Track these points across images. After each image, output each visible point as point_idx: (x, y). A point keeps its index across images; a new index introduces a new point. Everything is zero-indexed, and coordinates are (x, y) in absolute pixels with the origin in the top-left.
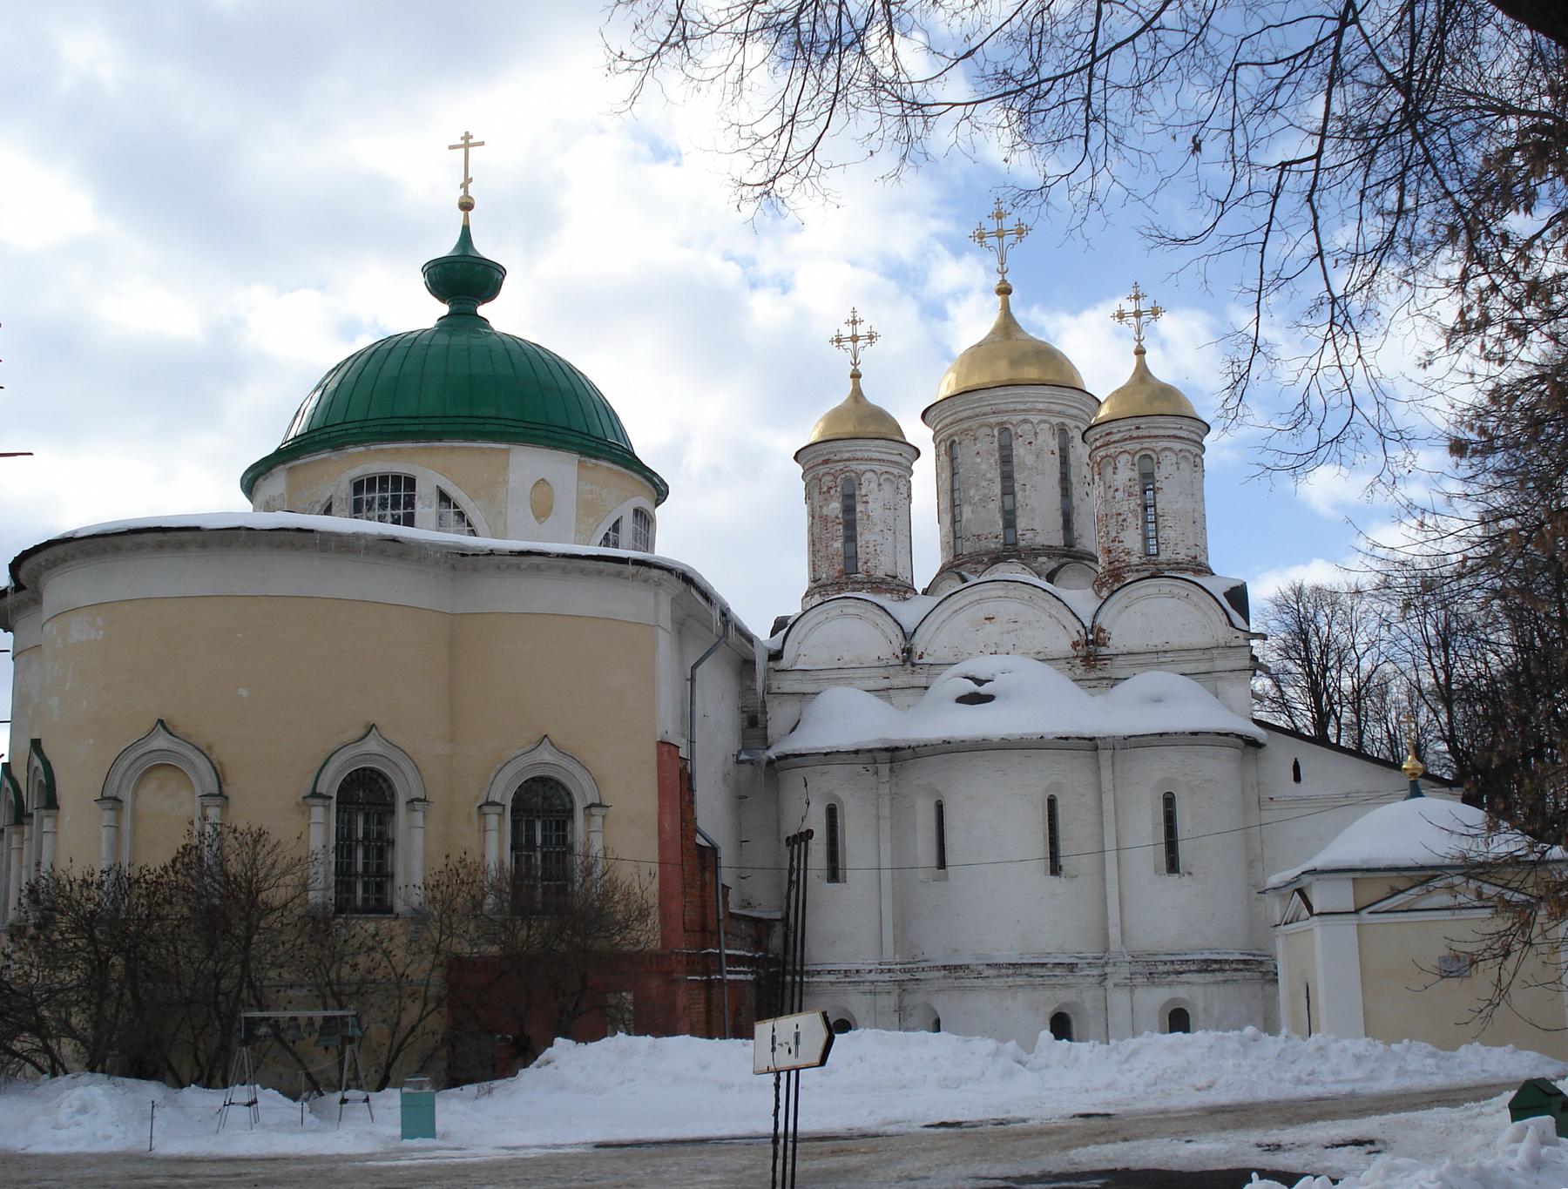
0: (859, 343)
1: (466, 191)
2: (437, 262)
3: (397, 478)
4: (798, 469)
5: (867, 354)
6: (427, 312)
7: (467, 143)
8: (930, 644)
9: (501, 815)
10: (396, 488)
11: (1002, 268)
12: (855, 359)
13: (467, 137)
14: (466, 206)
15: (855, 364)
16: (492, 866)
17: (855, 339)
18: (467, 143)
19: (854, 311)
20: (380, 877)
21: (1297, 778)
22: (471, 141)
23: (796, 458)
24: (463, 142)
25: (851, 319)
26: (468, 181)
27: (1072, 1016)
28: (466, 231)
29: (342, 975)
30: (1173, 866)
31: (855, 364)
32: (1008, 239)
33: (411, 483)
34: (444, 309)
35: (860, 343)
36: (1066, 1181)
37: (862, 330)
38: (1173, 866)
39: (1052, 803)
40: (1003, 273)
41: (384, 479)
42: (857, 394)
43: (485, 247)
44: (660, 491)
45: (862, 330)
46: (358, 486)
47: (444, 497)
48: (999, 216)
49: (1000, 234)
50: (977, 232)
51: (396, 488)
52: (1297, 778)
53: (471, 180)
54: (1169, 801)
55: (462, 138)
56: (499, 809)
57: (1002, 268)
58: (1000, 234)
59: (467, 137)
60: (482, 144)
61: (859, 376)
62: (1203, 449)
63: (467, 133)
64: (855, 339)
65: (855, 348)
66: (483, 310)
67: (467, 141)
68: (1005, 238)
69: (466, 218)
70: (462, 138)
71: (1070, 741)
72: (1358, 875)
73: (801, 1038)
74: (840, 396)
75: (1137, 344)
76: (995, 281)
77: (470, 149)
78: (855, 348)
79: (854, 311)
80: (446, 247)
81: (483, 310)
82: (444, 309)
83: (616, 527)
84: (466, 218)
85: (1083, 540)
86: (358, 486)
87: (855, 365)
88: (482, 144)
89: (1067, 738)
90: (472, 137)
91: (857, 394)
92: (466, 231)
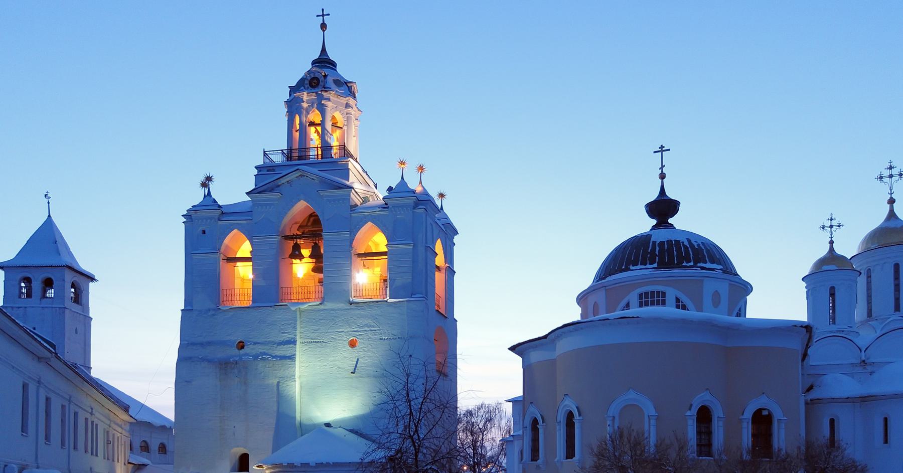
0: (833, 228)
1: (662, 171)
3: (658, 292)
4: (804, 284)
6: (645, 224)
7: (662, 149)
9: (748, 423)
11: (891, 192)
12: (891, 190)
13: (662, 147)
14: (662, 176)
16: (652, 444)
17: (831, 227)
18: (662, 149)
20: (709, 445)
22: (663, 149)
23: (803, 279)
24: (660, 150)
26: (663, 166)
33: (664, 294)
34: (654, 222)
35: (833, 229)
37: (835, 223)
41: (653, 292)
42: (832, 249)
43: (671, 194)
45: (835, 223)
46: (640, 296)
47: (678, 300)
50: (879, 176)
51: (652, 297)
55: (660, 148)
57: (891, 192)
59: (662, 147)
60: (669, 150)
61: (833, 242)
63: (662, 145)
64: (831, 227)
66: (670, 221)
67: (662, 150)
69: (662, 182)
70: (660, 148)
71: (849, 399)
74: (824, 251)
77: (663, 153)
80: (653, 196)
81: (670, 221)
82: (654, 222)
83: (740, 309)
84: (662, 182)
86: (640, 296)
87: (831, 238)
88: (669, 150)
89: (834, 399)
90: (664, 147)
91: (832, 249)
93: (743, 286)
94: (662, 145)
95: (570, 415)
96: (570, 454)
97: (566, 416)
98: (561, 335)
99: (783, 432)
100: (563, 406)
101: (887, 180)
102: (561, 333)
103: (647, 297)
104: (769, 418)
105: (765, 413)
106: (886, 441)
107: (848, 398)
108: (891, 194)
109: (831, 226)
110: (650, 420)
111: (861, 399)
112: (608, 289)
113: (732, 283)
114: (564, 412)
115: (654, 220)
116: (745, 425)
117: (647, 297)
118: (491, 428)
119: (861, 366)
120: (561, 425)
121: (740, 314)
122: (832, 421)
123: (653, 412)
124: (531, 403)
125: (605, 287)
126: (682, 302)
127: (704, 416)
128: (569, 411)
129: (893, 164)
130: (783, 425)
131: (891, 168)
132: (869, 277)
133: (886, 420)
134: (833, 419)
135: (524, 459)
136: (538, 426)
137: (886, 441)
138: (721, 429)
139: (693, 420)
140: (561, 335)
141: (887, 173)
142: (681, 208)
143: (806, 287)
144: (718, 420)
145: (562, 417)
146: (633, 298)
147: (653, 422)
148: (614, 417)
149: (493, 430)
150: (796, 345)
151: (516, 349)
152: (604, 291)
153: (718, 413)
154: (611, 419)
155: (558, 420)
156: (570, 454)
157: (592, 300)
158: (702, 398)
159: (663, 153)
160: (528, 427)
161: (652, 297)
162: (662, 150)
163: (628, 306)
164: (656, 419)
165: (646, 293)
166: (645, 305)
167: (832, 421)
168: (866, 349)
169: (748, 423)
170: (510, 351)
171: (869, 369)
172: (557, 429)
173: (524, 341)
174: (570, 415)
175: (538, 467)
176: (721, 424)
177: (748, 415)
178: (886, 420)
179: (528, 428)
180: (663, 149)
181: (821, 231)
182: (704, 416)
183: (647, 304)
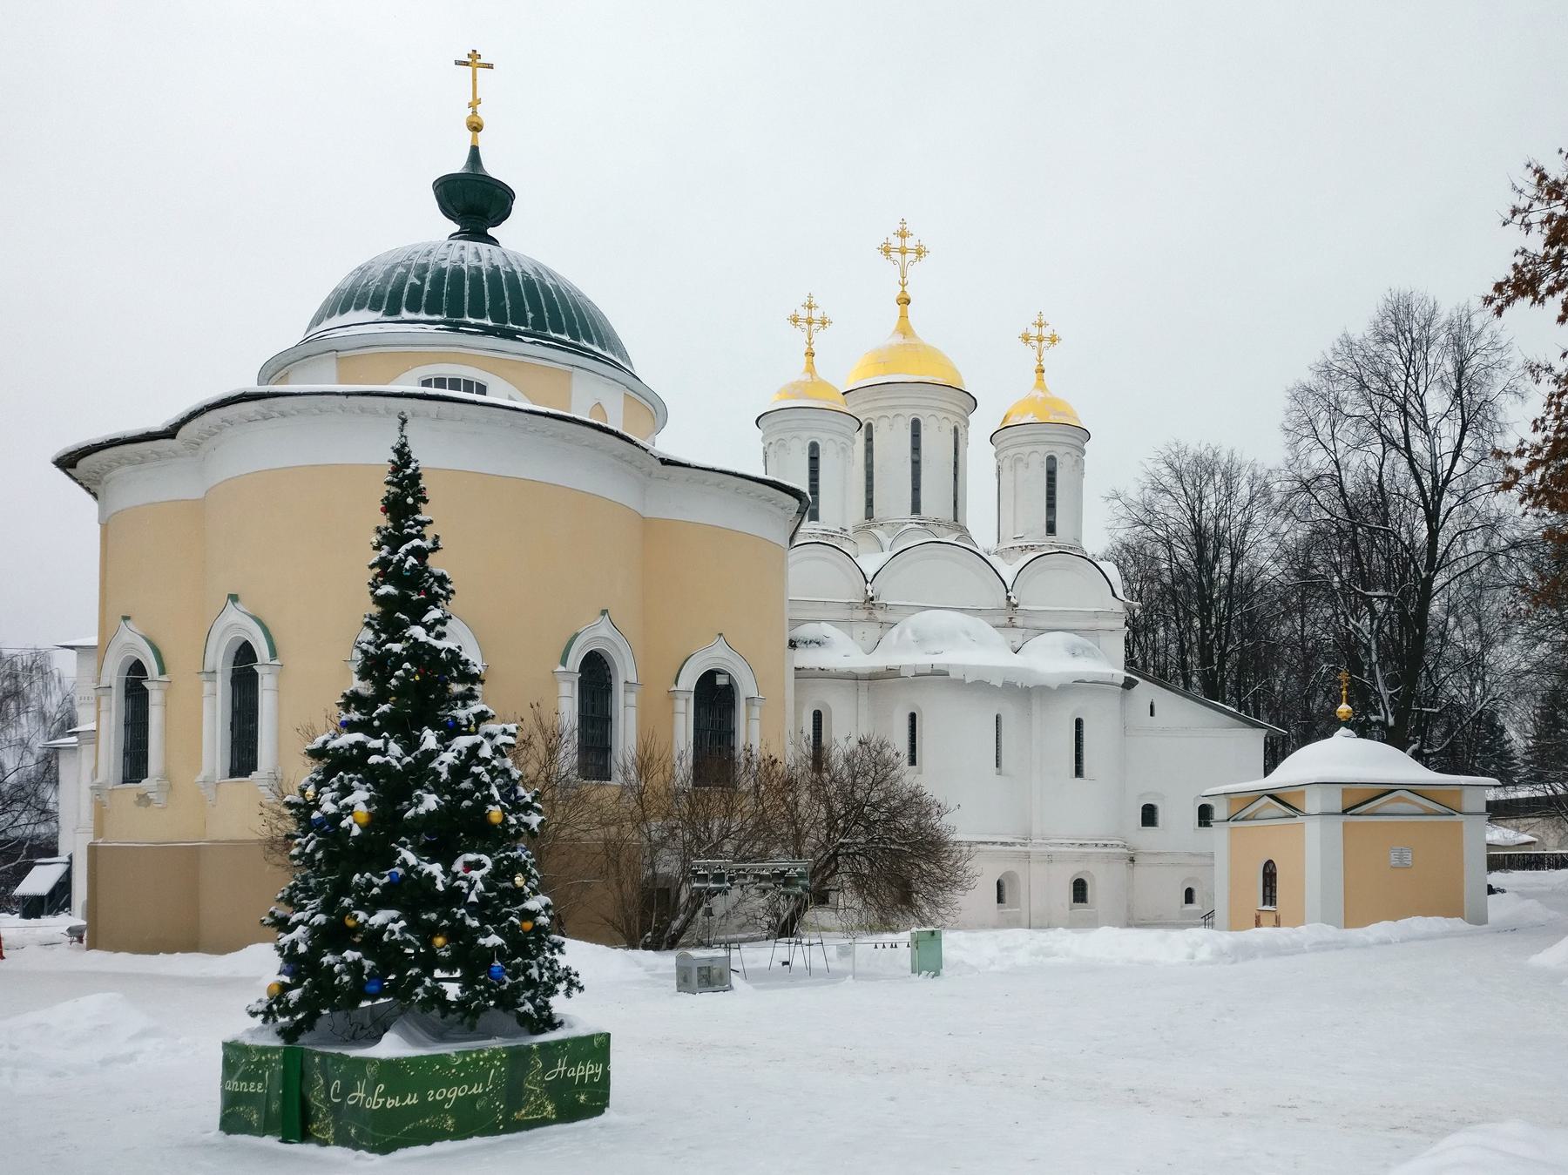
1: (475, 113)
2: (441, 181)
7: (473, 61)
8: (888, 592)
12: (810, 339)
13: (474, 55)
15: (810, 344)
18: (473, 61)
19: (810, 296)
21: (1152, 714)
24: (470, 60)
28: (475, 151)
29: (1414, 336)
30: (1079, 772)
31: (810, 344)
38: (1079, 772)
40: (903, 286)
43: (493, 167)
45: (910, 243)
48: (903, 235)
49: (903, 252)
54: (1079, 723)
56: (687, 696)
58: (903, 252)
59: (474, 55)
60: (490, 66)
62: (1084, 452)
65: (810, 329)
66: (491, 231)
68: (907, 255)
69: (475, 138)
72: (1344, 786)
73: (1156, 708)
78: (810, 329)
79: (810, 296)
80: (457, 164)
81: (491, 231)
85: (1357, 337)
88: (490, 66)
91: (904, 329)
92: (475, 151)
93: (651, 408)
95: (245, 653)
96: (243, 759)
98: (220, 428)
99: (755, 725)
101: (896, 256)
104: (730, 691)
105: (721, 681)
108: (903, 286)
109: (809, 320)
112: (342, 358)
113: (631, 393)
114: (227, 641)
118: (18, 714)
119: (864, 608)
124: (126, 618)
125: (337, 351)
130: (756, 712)
133: (913, 717)
134: (819, 711)
136: (146, 684)
138: (632, 712)
139: (573, 683)
140: (220, 428)
141: (804, 314)
143: (763, 440)
145: (219, 659)
149: (23, 719)
153: (625, 671)
156: (243, 759)
160: (114, 685)
168: (875, 575)
171: (879, 614)
173: (98, 541)
174: (245, 653)
175: (144, 800)
177: (689, 681)
178: (913, 717)
180: (478, 61)
181: (789, 326)
183: (127, 782)
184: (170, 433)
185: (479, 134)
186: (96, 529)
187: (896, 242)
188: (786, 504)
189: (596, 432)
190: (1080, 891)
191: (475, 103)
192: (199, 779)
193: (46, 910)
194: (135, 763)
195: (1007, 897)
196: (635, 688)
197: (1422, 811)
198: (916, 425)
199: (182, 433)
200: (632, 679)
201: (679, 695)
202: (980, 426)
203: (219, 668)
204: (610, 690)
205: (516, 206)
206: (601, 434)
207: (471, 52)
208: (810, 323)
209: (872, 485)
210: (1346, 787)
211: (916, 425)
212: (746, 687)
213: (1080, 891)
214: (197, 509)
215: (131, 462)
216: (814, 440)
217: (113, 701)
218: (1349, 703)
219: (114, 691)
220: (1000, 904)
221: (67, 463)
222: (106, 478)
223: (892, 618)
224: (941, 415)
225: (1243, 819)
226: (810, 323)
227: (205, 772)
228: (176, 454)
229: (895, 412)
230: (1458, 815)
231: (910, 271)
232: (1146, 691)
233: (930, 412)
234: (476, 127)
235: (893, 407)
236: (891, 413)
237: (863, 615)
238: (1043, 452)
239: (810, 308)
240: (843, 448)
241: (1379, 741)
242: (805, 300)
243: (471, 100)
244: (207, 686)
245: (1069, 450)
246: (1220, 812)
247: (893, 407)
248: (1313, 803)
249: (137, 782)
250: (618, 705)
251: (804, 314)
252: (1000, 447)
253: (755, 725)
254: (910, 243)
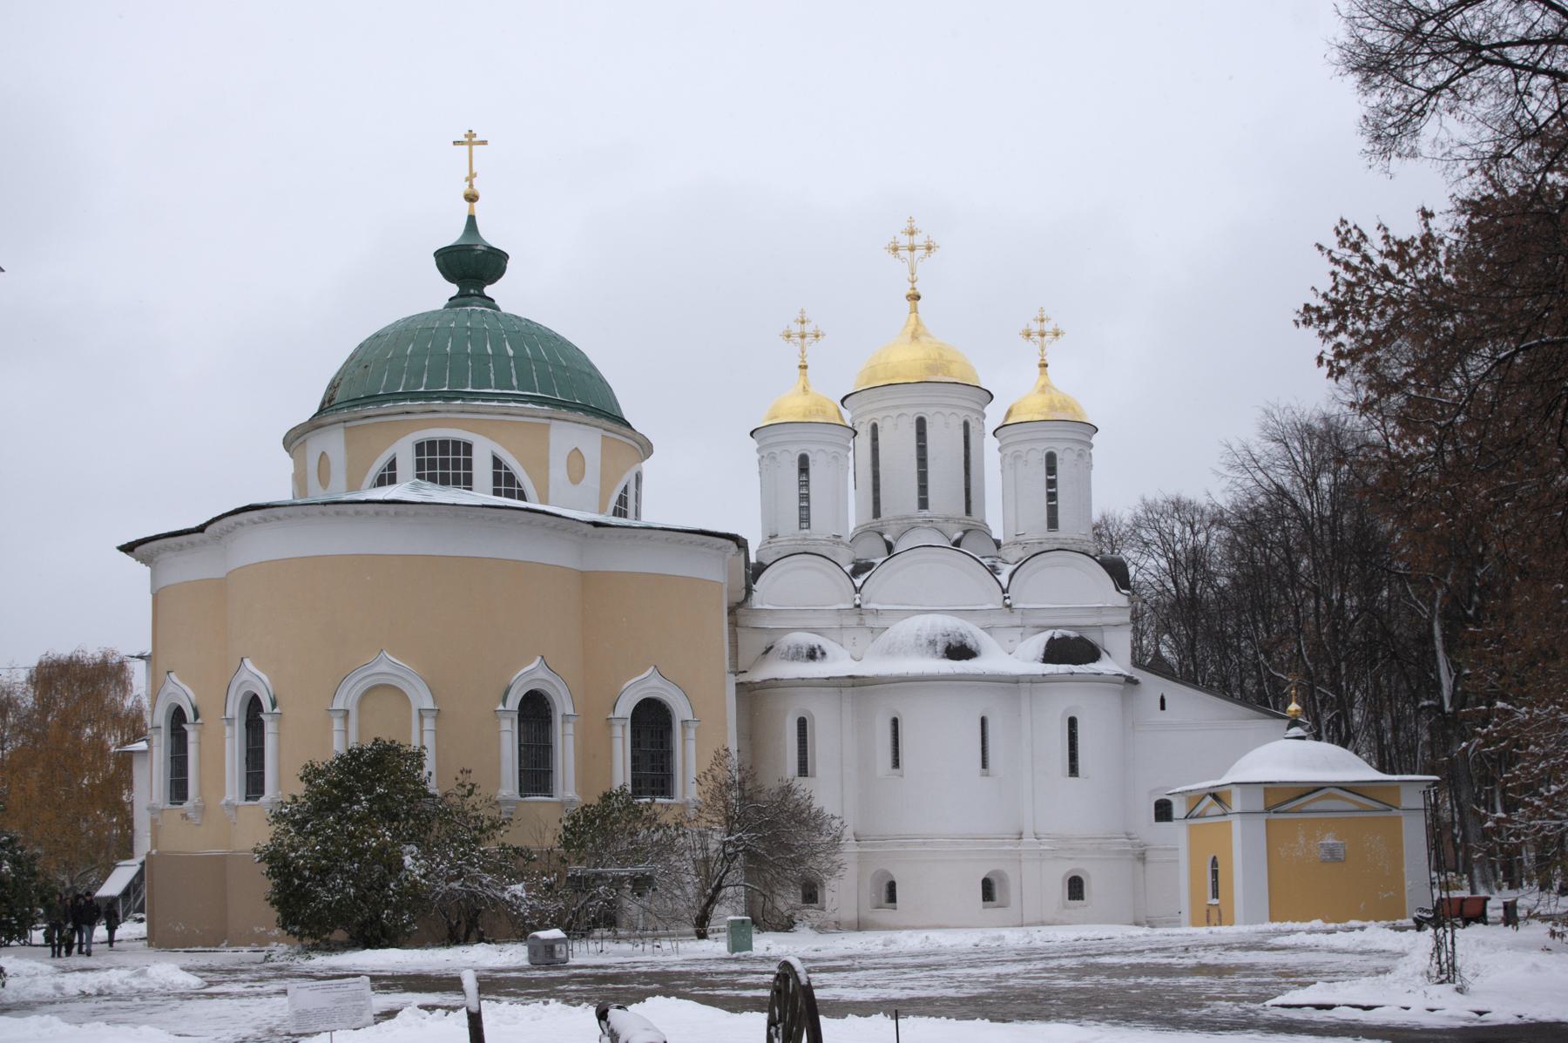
1: (471, 186)
3: (456, 443)
5: (814, 351)
7: (470, 140)
9: (624, 726)
10: (456, 452)
13: (471, 134)
14: (471, 198)
18: (470, 140)
21: (1163, 708)
22: (474, 139)
25: (800, 319)
27: (1080, 875)
28: (471, 220)
30: (1073, 770)
32: (918, 253)
33: (468, 448)
34: (453, 289)
35: (807, 339)
36: (745, 999)
37: (1048, 327)
38: (1073, 770)
39: (983, 721)
40: (913, 282)
41: (444, 443)
43: (492, 235)
44: (645, 448)
45: (919, 240)
46: (419, 448)
51: (444, 451)
52: (1163, 708)
53: (475, 175)
56: (623, 722)
59: (471, 134)
60: (484, 143)
67: (470, 140)
68: (916, 252)
69: (471, 209)
70: (466, 136)
72: (1267, 786)
75: (910, 285)
76: (1038, 361)
80: (452, 235)
81: (489, 290)
83: (626, 488)
84: (471, 209)
88: (484, 143)
92: (471, 220)
94: (470, 131)
96: (254, 786)
97: (245, 712)
99: (692, 746)
100: (238, 684)
101: (905, 254)
102: (233, 525)
103: (432, 451)
106: (896, 763)
107: (828, 679)
108: (913, 282)
110: (421, 718)
111: (851, 680)
115: (455, 285)
116: (618, 731)
117: (432, 451)
120: (233, 725)
121: (626, 498)
122: (802, 724)
123: (428, 704)
126: (506, 468)
127: (535, 710)
128: (250, 697)
129: (916, 226)
130: (692, 733)
131: (912, 233)
132: (875, 439)
133: (895, 722)
135: (154, 798)
136: (185, 726)
137: (896, 763)
138: (570, 741)
139: (512, 720)
140: (234, 528)
142: (511, 265)
143: (758, 451)
144: (563, 722)
145: (235, 709)
146: (404, 455)
147: (429, 724)
148: (347, 712)
150: (716, 570)
151: (137, 550)
152: (342, 435)
153: (563, 705)
154: (341, 714)
155: (229, 715)
156: (254, 786)
157: (316, 445)
158: (530, 674)
159: (475, 148)
161: (444, 451)
162: (470, 140)
163: (388, 477)
164: (436, 718)
165: (432, 443)
166: (448, 441)
167: (802, 724)
169: (624, 726)
170: (123, 553)
171: (870, 621)
172: (227, 735)
175: (185, 816)
176: (570, 728)
177: (625, 709)
178: (895, 722)
179: (163, 730)
180: (474, 139)
182: (535, 710)
184: (201, 529)
185: (475, 204)
186: (150, 597)
187: (905, 240)
188: (719, 545)
189: (526, 513)
190: (1076, 888)
191: (471, 178)
192: (223, 802)
193: (121, 918)
194: (178, 790)
195: (997, 894)
196: (571, 719)
197: (1356, 807)
198: (921, 424)
199: (208, 530)
200: (570, 711)
201: (614, 722)
202: (994, 415)
203: (237, 715)
204: (550, 722)
205: (510, 264)
206: (532, 515)
207: (467, 133)
208: (803, 337)
209: (878, 485)
210: (1269, 788)
211: (921, 424)
212: (681, 710)
213: (1076, 888)
214: (219, 587)
215: (172, 549)
216: (805, 452)
217: (163, 736)
218: (1297, 702)
219: (163, 730)
220: (986, 903)
221: (128, 548)
222: (156, 559)
223: (881, 623)
224: (947, 411)
225: (1198, 817)
226: (803, 337)
227: (229, 797)
228: (204, 542)
229: (898, 412)
230: (1395, 811)
231: (808, 350)
232: (1153, 685)
233: (935, 409)
234: (471, 198)
235: (897, 407)
236: (895, 413)
237: (853, 621)
238: (1042, 449)
239: (803, 322)
240: (834, 457)
241: (1331, 741)
242: (905, 225)
243: (467, 174)
244: (228, 730)
245: (1070, 445)
246: (1179, 810)
247: (897, 407)
248: (1236, 804)
249: (181, 804)
250: (556, 734)
251: (796, 328)
252: (1004, 443)
253: (692, 746)
254: (919, 240)
